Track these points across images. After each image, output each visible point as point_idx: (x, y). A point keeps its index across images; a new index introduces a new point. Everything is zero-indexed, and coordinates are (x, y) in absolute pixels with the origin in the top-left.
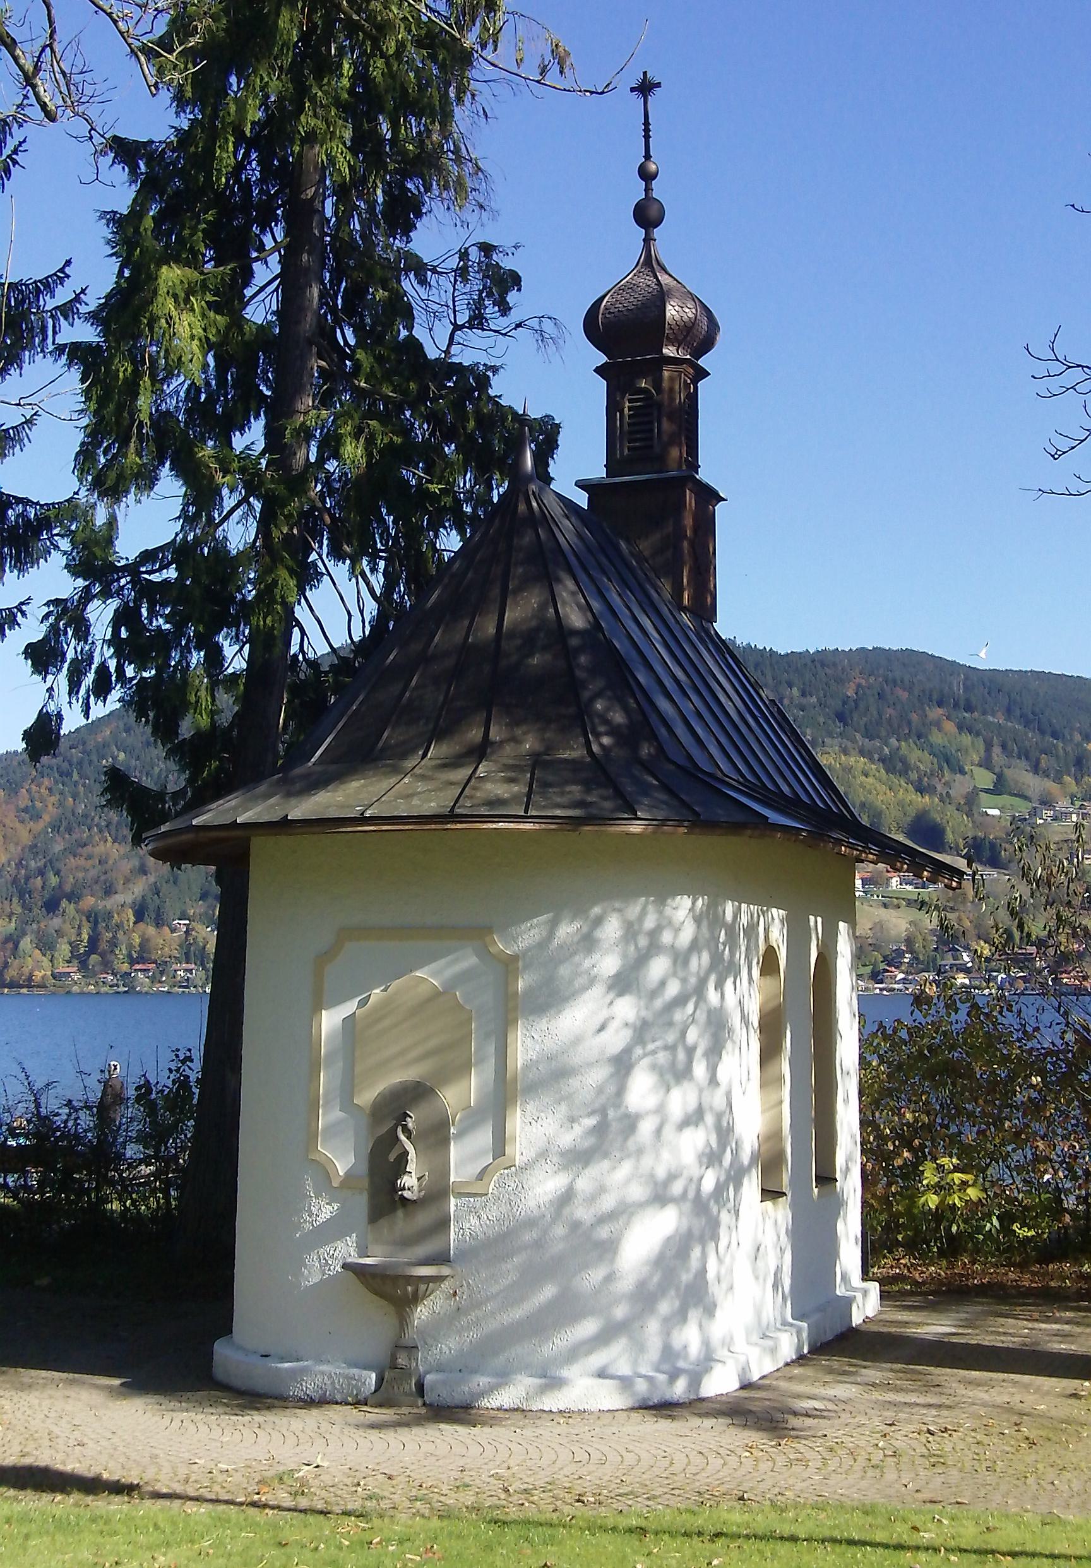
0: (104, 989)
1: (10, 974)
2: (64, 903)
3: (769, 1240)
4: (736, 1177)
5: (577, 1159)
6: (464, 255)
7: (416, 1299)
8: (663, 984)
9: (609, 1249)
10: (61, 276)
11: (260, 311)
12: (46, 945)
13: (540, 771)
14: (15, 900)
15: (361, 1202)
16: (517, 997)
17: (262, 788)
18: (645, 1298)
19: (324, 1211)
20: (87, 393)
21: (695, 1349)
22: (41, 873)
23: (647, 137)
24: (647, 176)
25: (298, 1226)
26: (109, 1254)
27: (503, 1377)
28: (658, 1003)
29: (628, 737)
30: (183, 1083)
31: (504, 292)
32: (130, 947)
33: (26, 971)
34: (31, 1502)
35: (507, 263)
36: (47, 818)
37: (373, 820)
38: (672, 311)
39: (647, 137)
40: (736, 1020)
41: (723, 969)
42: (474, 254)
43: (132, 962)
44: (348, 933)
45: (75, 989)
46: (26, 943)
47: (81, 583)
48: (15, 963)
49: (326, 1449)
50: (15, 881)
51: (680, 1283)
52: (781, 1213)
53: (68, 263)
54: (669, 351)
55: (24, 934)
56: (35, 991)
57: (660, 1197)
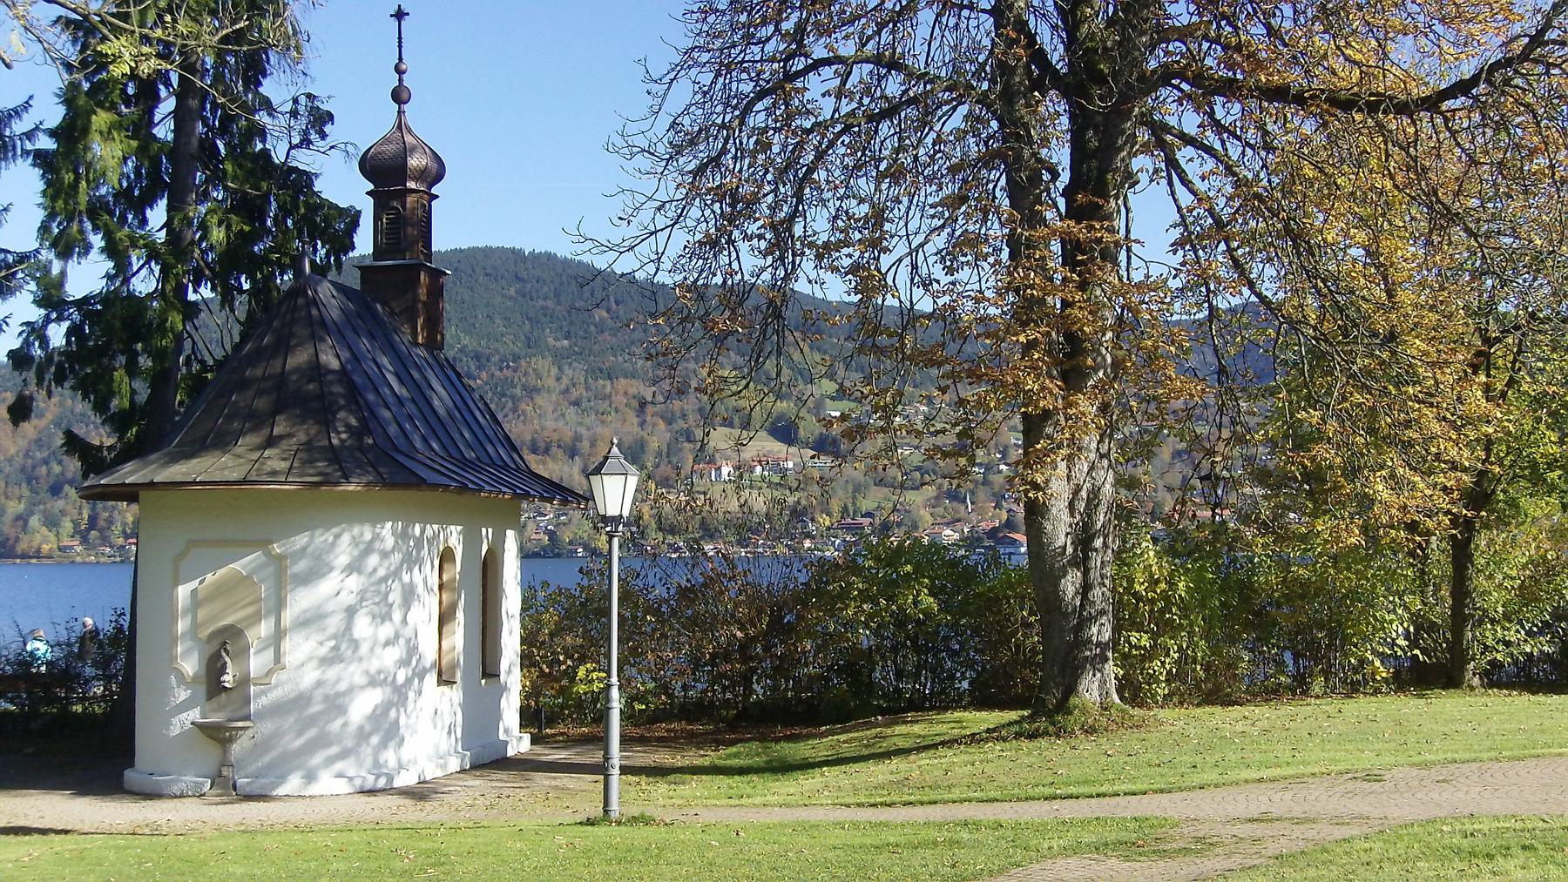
0: (102, 560)
1: (22, 547)
2: (67, 488)
3: (445, 708)
4: (421, 675)
5: (326, 662)
6: (295, 101)
7: (231, 740)
8: (375, 570)
9: (342, 710)
10: (26, 106)
11: (164, 131)
12: (52, 523)
13: (310, 452)
14: (24, 485)
15: (202, 690)
16: (283, 579)
17: (154, 456)
18: (362, 736)
19: (183, 695)
20: (44, 193)
21: (392, 763)
22: (46, 462)
23: (400, 47)
24: (400, 71)
25: (168, 704)
26: (61, 725)
27: (282, 778)
28: (373, 579)
29: (357, 433)
30: (120, 629)
31: (324, 124)
32: (124, 524)
33: (35, 544)
34: (11, 838)
35: (324, 107)
36: (49, 416)
37: (201, 483)
38: (414, 162)
39: (400, 47)
40: (420, 589)
41: (411, 561)
42: (303, 100)
43: (127, 537)
44: (194, 543)
45: (78, 559)
46: (34, 521)
47: (43, 312)
48: (25, 538)
49: (186, 816)
50: (23, 470)
51: (384, 726)
52: (455, 694)
53: (31, 97)
54: (411, 185)
55: (32, 513)
56: (44, 561)
57: (373, 682)
